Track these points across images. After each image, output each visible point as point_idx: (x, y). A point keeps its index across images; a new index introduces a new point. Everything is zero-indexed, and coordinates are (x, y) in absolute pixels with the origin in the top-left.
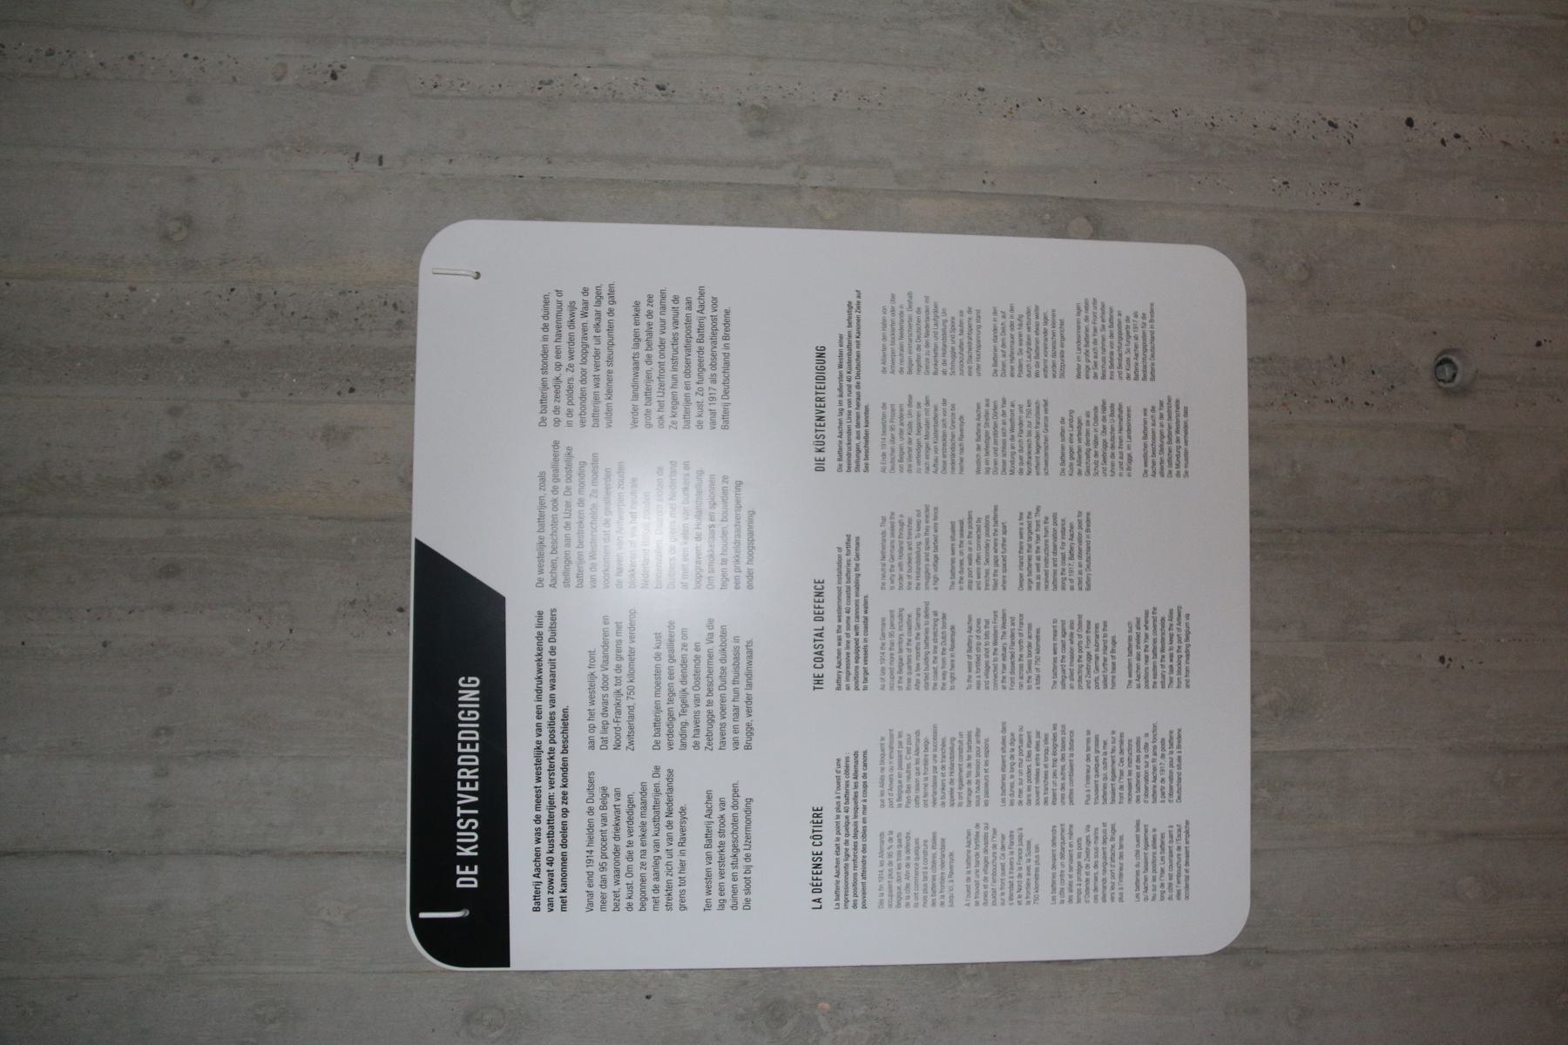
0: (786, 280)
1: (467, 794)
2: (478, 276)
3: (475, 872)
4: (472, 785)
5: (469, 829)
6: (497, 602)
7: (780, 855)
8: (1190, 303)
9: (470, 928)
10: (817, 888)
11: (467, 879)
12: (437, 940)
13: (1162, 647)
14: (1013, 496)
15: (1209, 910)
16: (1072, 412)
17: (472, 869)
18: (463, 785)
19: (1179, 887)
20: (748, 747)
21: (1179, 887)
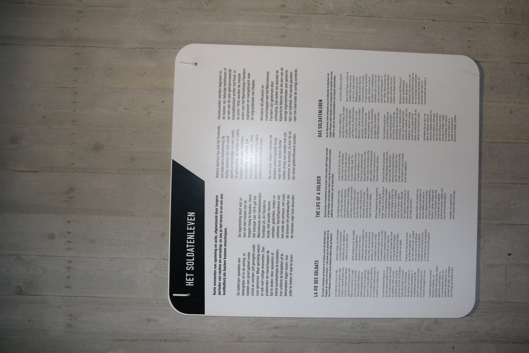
0: (312, 65)
1: (190, 265)
2: (196, 64)
3: (193, 280)
4: (193, 219)
5: (189, 266)
6: (203, 182)
7: (303, 276)
8: (450, 80)
9: (189, 296)
10: (316, 288)
11: (190, 282)
12: (179, 304)
13: (434, 204)
14: (379, 146)
15: (457, 302)
16: (418, 269)
17: (191, 279)
18: (189, 219)
19: (449, 293)
20: (292, 237)
21: (449, 293)
